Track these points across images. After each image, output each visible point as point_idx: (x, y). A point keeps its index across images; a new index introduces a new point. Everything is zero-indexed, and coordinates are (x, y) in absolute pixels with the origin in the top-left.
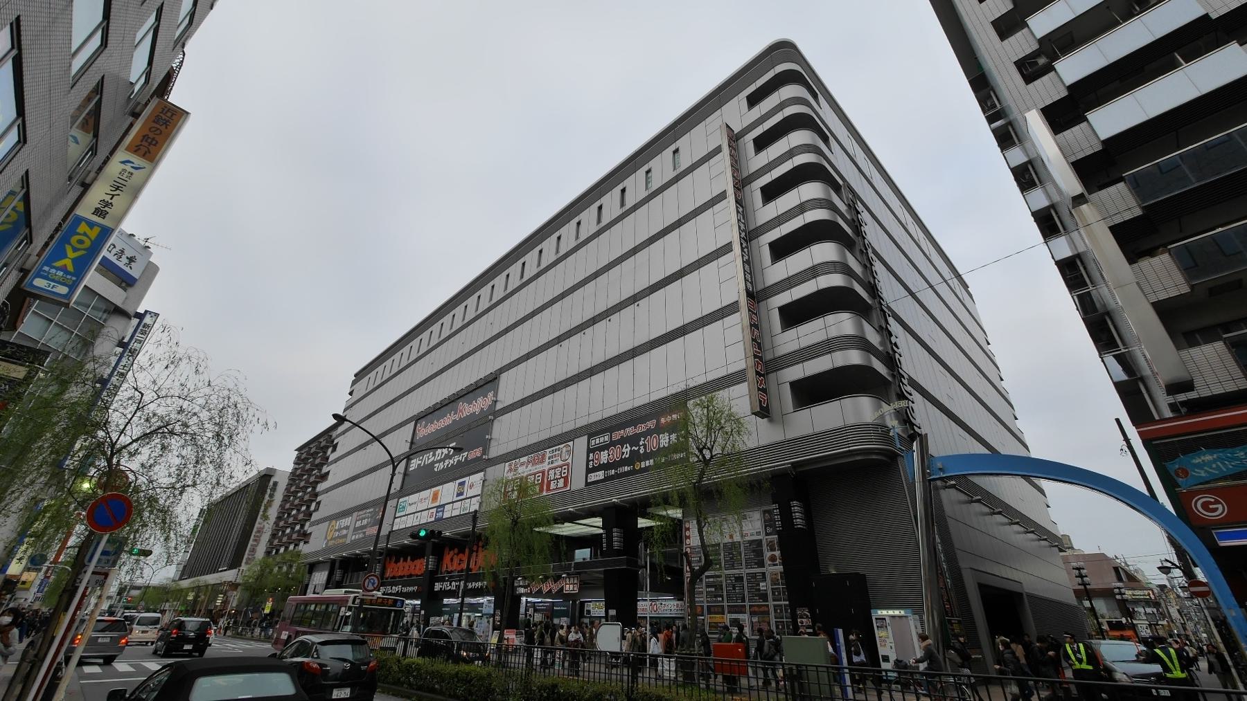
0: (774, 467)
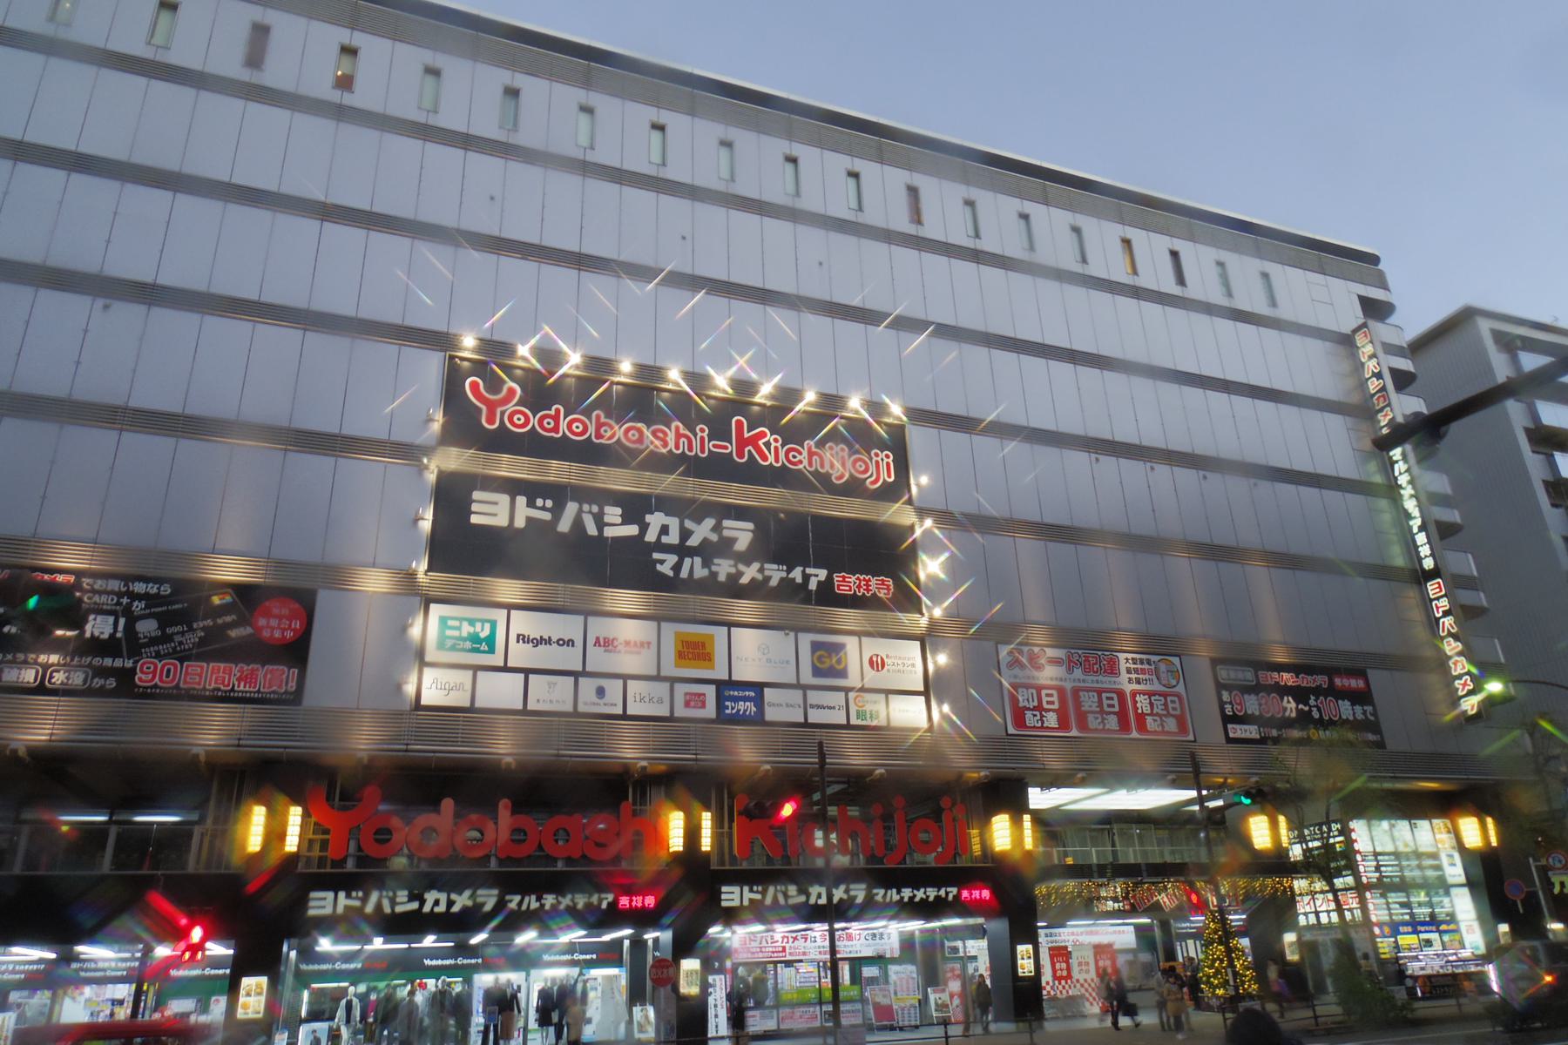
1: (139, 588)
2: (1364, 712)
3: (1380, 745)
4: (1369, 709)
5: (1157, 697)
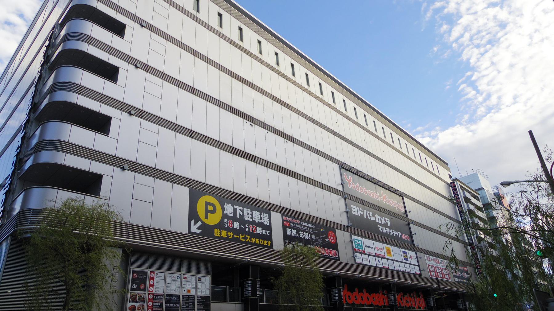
0: (401, 281)
1: (310, 225)
2: (266, 233)
3: (271, 247)
4: (268, 232)
5: (149, 297)
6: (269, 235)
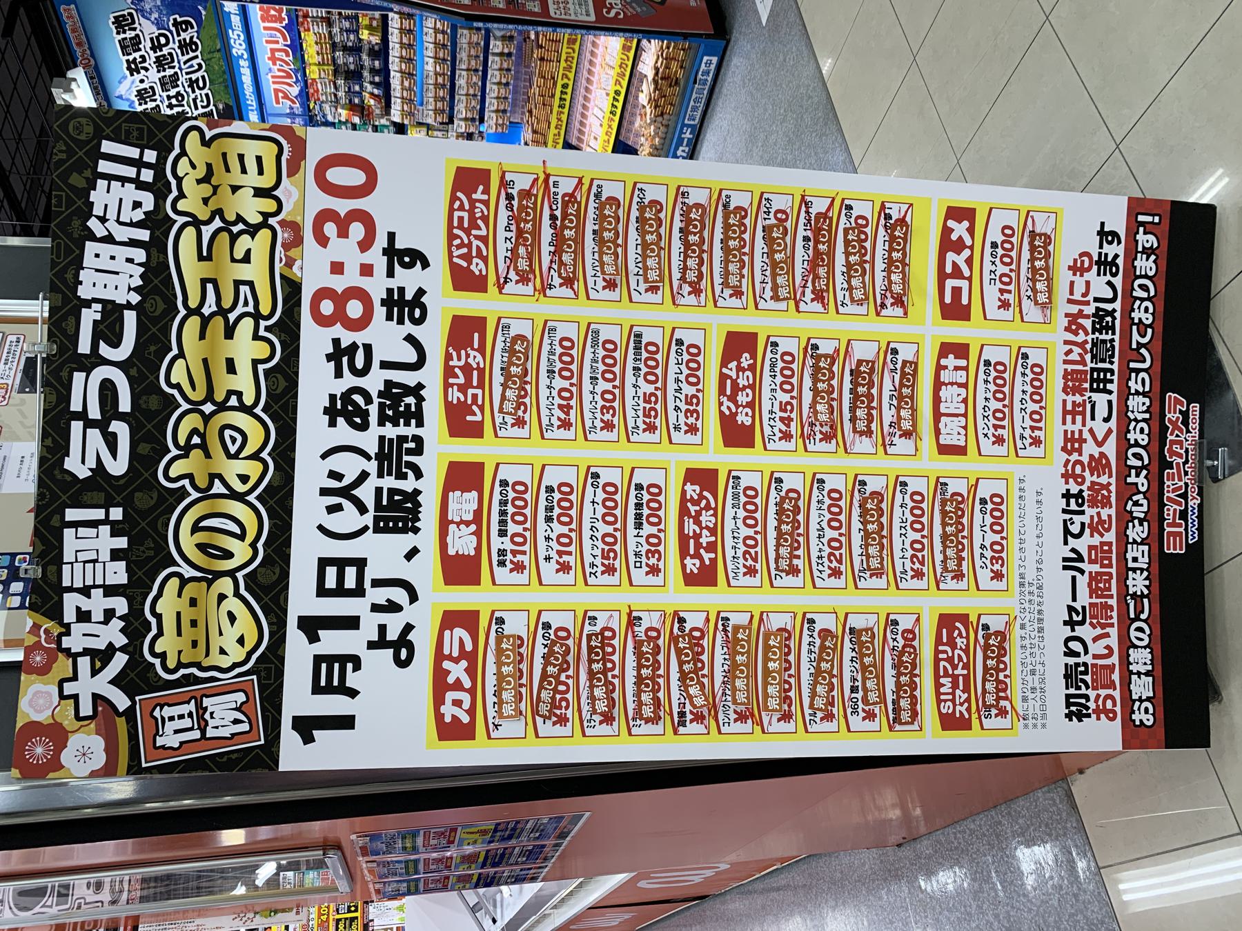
6: (459, 194)
